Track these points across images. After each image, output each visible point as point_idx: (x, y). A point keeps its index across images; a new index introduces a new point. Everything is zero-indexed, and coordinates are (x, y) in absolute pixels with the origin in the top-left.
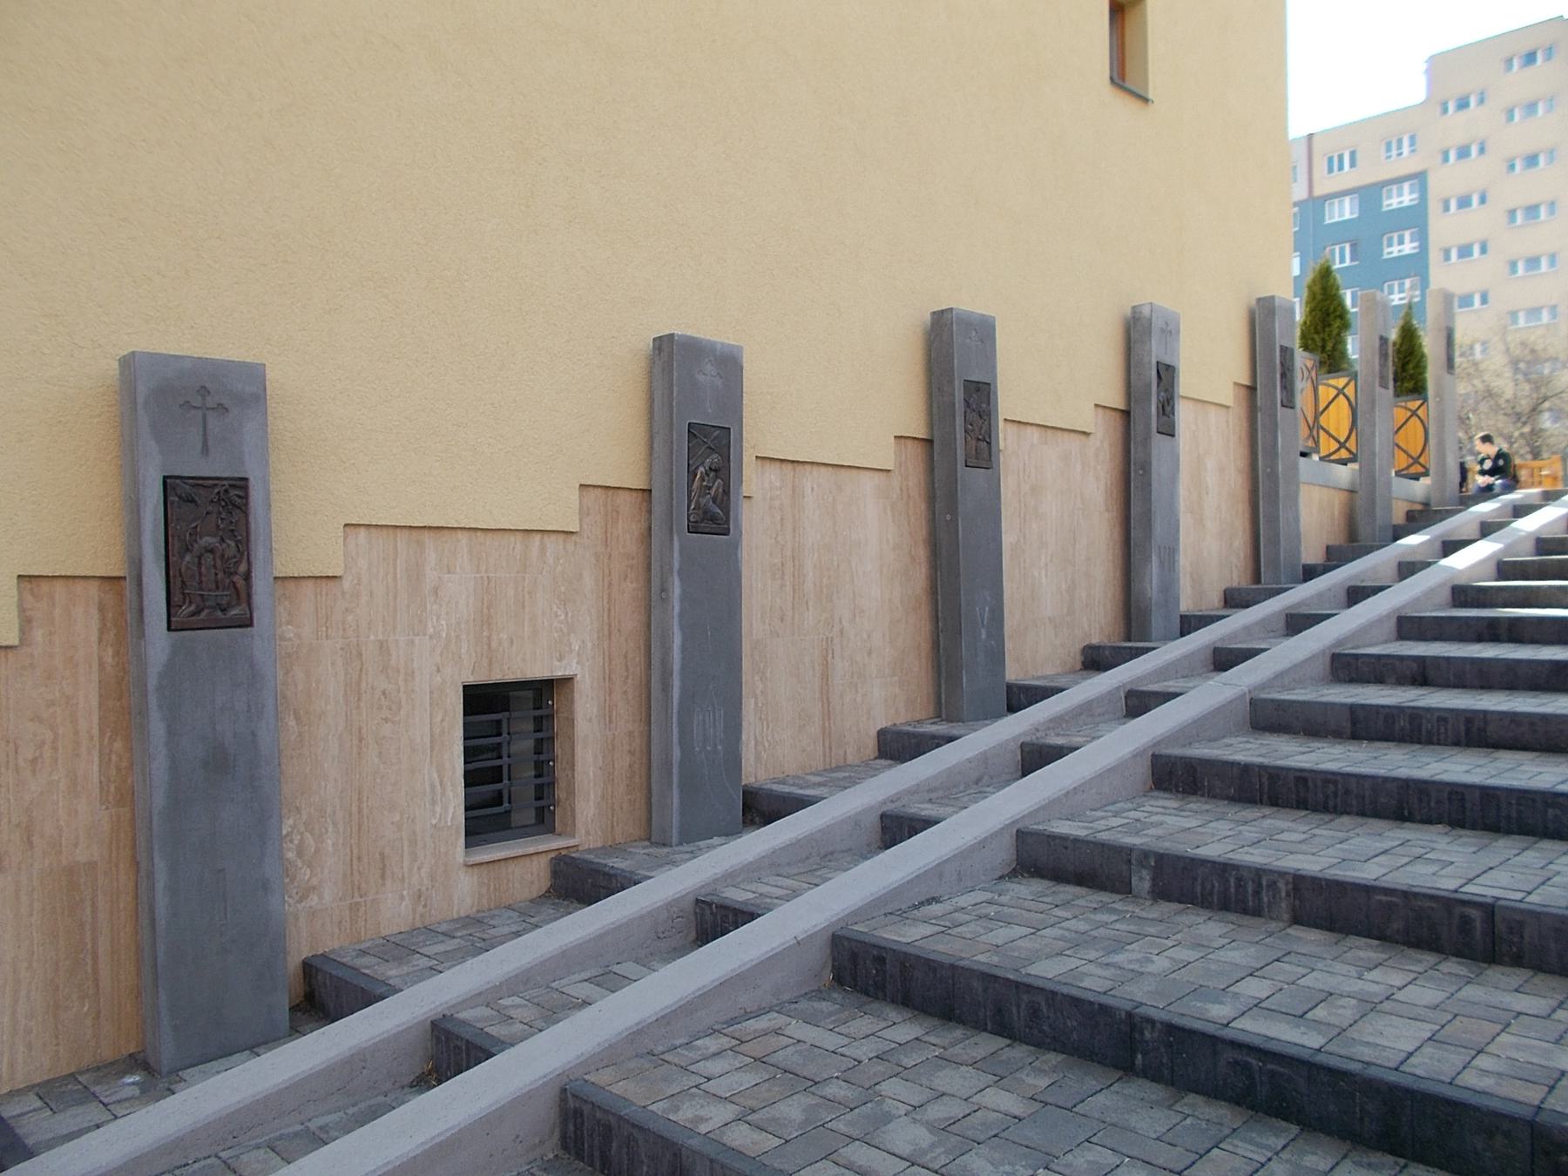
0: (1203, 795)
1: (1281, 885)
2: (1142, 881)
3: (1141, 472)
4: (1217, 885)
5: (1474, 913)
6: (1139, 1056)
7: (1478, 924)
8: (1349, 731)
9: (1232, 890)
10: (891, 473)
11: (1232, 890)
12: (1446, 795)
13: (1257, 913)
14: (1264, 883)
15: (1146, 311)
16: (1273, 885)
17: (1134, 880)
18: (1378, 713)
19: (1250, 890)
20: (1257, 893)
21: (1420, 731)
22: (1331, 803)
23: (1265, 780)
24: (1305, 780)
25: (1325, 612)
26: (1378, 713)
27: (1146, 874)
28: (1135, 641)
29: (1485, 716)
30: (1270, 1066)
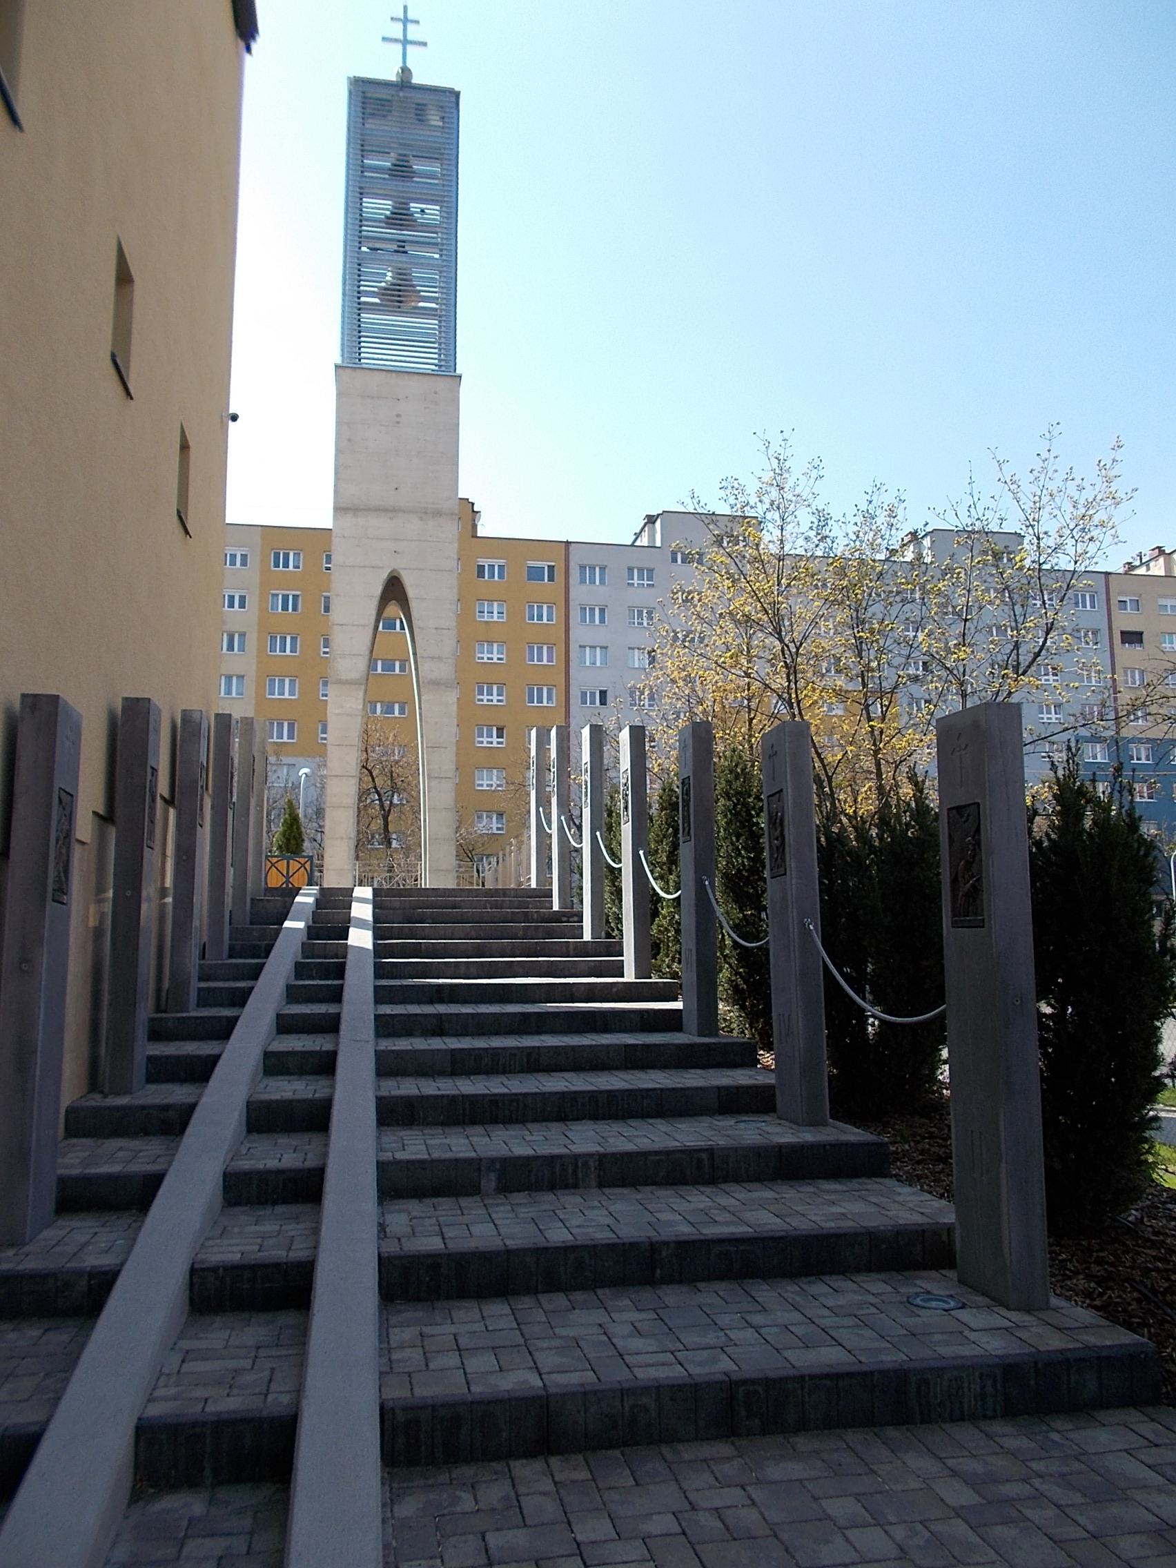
0: (418, 1125)
1: (591, 1163)
2: (489, 1182)
3: (184, 858)
4: (546, 1172)
5: (704, 1156)
6: (658, 1271)
7: (706, 1162)
8: (449, 1070)
9: (558, 1174)
10: (86, 847)
11: (558, 1174)
12: (587, 1099)
13: (576, 1186)
14: (580, 1164)
15: (196, 716)
16: (586, 1164)
17: (483, 1183)
18: (471, 1055)
19: (570, 1171)
20: (575, 1172)
21: (498, 1064)
22: (514, 1116)
23: (467, 1106)
24: (496, 1102)
25: (821, 969)
26: (471, 1055)
27: (493, 1176)
28: (172, 1012)
29: (452, 1056)
30: (742, 1248)
